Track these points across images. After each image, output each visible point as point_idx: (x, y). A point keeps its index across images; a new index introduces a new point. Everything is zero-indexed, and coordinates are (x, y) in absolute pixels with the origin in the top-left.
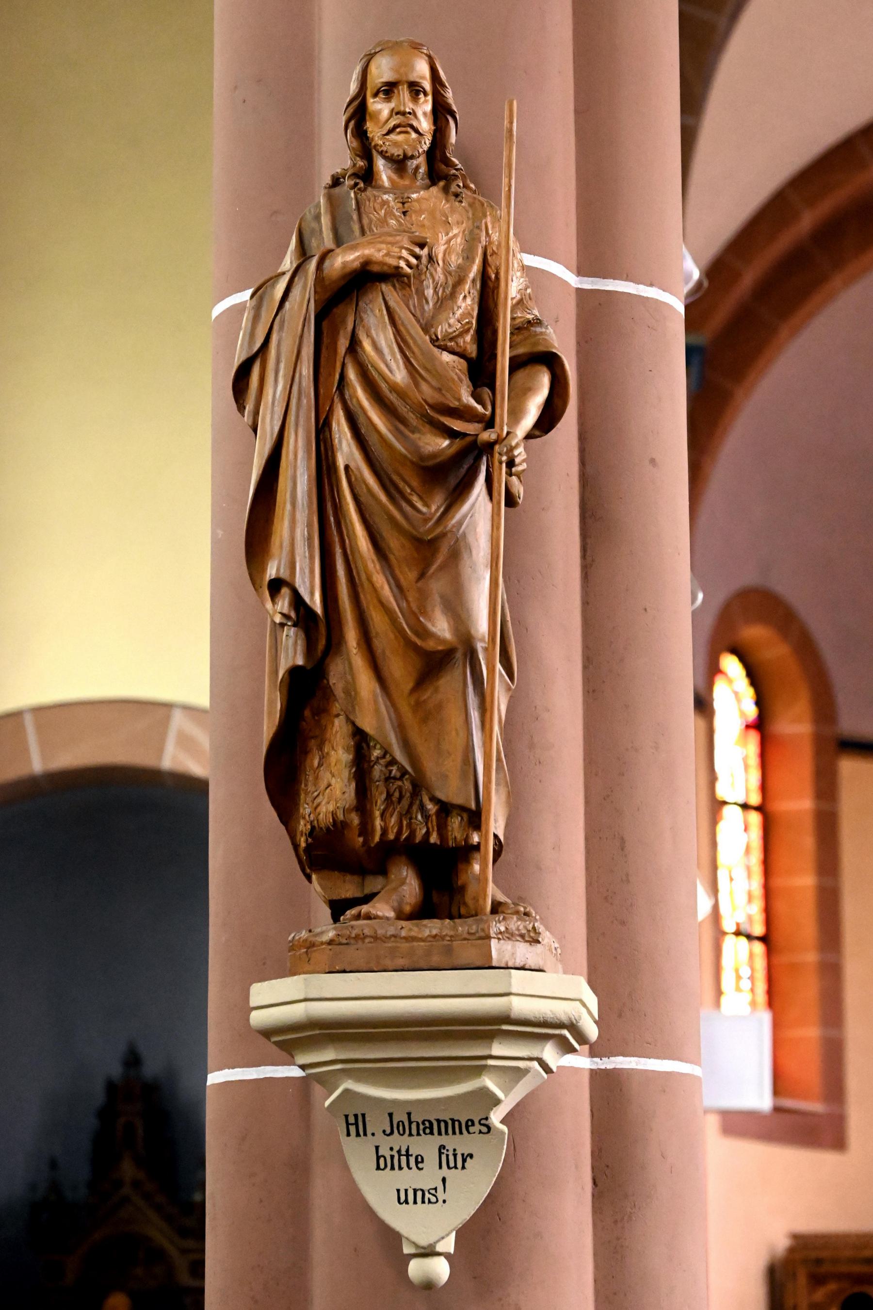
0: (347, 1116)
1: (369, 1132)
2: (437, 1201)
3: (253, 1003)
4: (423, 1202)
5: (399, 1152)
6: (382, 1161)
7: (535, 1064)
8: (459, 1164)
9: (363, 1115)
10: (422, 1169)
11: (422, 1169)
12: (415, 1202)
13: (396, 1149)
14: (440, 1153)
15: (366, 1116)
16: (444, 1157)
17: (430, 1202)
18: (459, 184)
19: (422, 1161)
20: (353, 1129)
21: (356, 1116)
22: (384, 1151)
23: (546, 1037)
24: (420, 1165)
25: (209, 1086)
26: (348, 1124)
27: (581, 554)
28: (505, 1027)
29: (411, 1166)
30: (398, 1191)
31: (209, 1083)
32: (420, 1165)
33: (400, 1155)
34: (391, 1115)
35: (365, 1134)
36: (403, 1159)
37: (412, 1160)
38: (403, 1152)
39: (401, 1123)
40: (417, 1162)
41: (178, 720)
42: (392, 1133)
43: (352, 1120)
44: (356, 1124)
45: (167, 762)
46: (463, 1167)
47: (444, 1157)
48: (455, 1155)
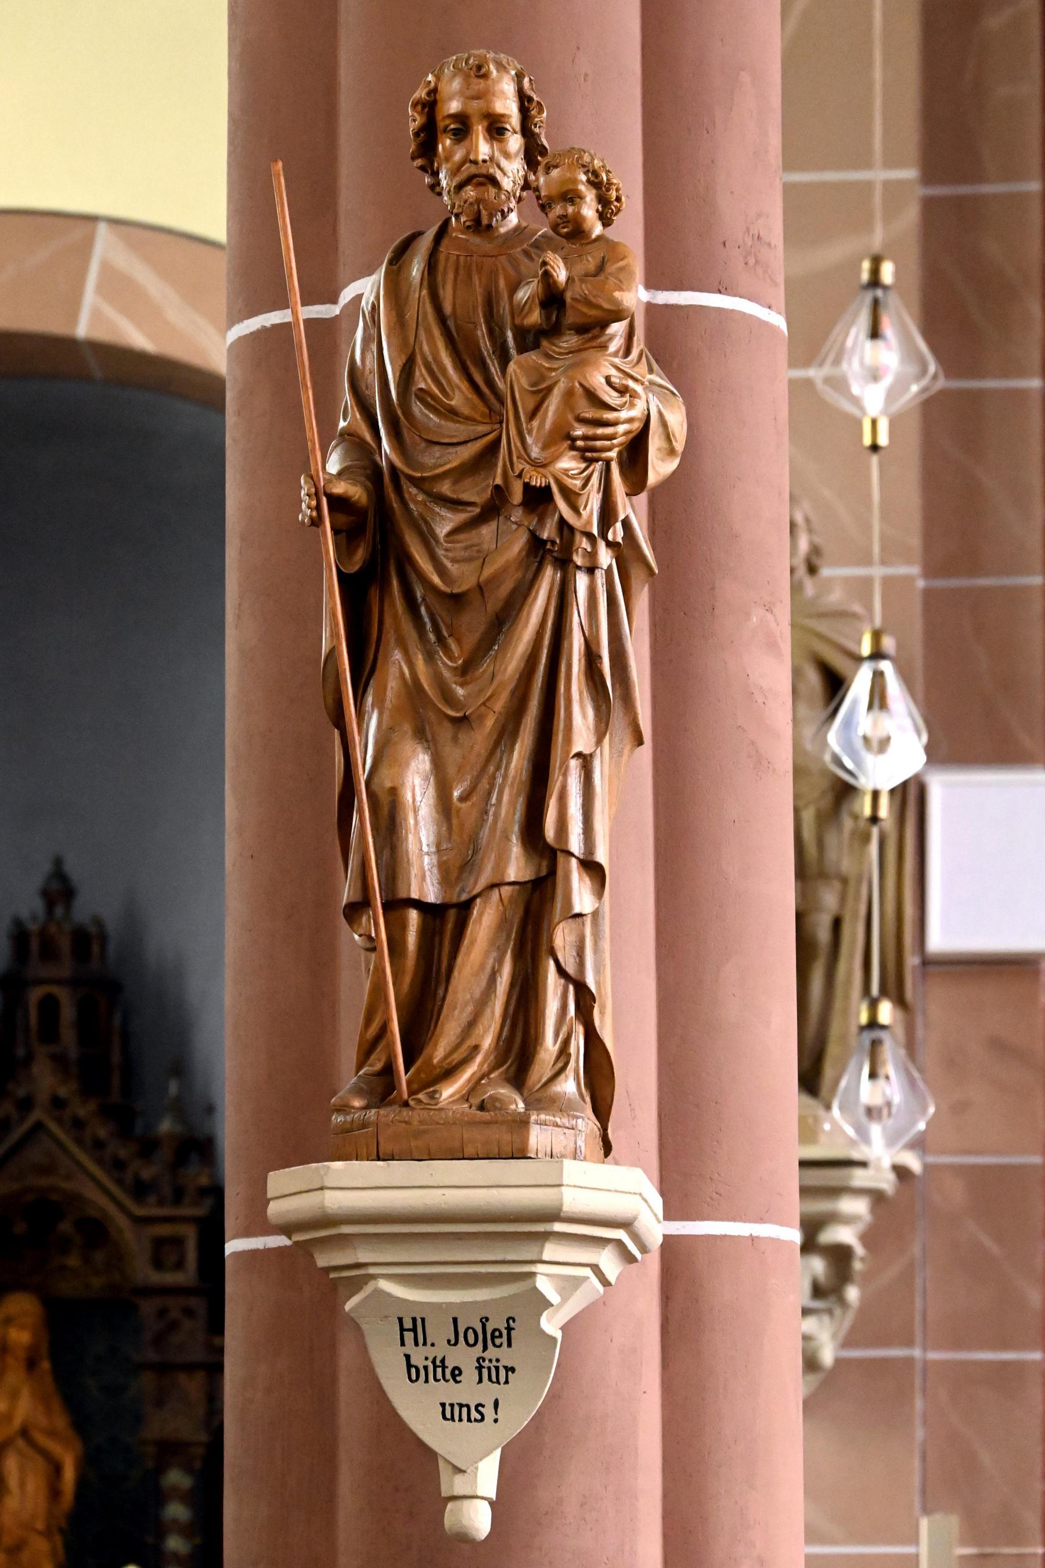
0: (400, 1320)
1: (429, 1342)
2: (483, 1419)
3: (269, 1195)
4: (469, 1420)
5: (434, 1362)
6: (413, 1370)
7: (587, 1272)
8: (502, 1379)
9: (423, 1320)
10: (460, 1382)
11: (460, 1382)
12: (460, 1420)
13: (431, 1359)
14: (480, 1368)
15: (458, 1320)
16: (485, 1372)
17: (476, 1420)
18: (420, 387)
19: (460, 1373)
20: (409, 1336)
21: (414, 1320)
22: (417, 1360)
23: (603, 1242)
24: (458, 1378)
25: (228, 1256)
26: (402, 1330)
27: (871, 318)
28: (558, 1227)
29: (438, 1378)
30: (443, 1405)
31: (227, 1252)
32: (458, 1378)
33: (435, 1367)
34: (455, 1320)
35: (425, 1344)
36: (439, 1370)
37: (448, 1372)
38: (438, 1363)
39: (471, 1331)
40: (493, 1337)
41: (103, 234)
42: (456, 1343)
43: (408, 1324)
44: (414, 1330)
45: (82, 330)
46: (507, 1382)
47: (485, 1372)
48: (497, 1368)
